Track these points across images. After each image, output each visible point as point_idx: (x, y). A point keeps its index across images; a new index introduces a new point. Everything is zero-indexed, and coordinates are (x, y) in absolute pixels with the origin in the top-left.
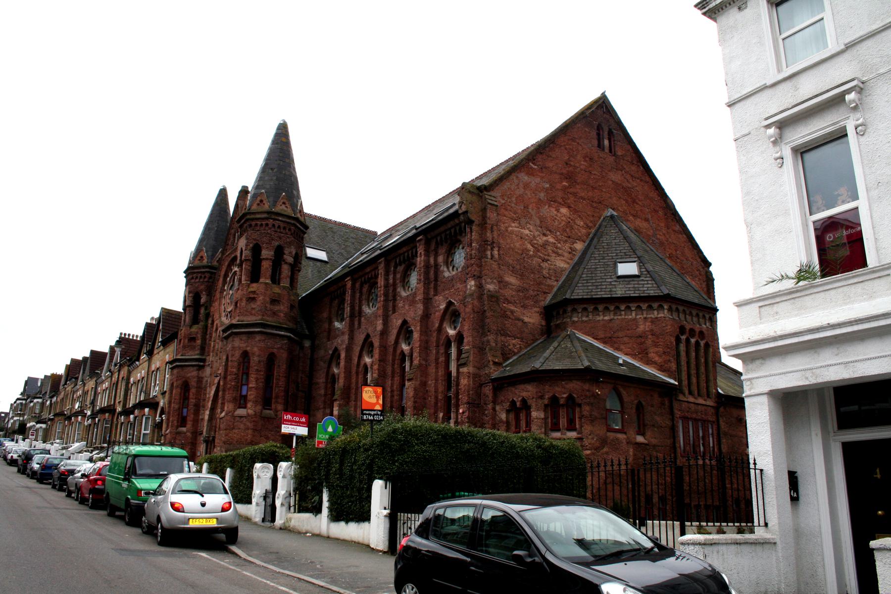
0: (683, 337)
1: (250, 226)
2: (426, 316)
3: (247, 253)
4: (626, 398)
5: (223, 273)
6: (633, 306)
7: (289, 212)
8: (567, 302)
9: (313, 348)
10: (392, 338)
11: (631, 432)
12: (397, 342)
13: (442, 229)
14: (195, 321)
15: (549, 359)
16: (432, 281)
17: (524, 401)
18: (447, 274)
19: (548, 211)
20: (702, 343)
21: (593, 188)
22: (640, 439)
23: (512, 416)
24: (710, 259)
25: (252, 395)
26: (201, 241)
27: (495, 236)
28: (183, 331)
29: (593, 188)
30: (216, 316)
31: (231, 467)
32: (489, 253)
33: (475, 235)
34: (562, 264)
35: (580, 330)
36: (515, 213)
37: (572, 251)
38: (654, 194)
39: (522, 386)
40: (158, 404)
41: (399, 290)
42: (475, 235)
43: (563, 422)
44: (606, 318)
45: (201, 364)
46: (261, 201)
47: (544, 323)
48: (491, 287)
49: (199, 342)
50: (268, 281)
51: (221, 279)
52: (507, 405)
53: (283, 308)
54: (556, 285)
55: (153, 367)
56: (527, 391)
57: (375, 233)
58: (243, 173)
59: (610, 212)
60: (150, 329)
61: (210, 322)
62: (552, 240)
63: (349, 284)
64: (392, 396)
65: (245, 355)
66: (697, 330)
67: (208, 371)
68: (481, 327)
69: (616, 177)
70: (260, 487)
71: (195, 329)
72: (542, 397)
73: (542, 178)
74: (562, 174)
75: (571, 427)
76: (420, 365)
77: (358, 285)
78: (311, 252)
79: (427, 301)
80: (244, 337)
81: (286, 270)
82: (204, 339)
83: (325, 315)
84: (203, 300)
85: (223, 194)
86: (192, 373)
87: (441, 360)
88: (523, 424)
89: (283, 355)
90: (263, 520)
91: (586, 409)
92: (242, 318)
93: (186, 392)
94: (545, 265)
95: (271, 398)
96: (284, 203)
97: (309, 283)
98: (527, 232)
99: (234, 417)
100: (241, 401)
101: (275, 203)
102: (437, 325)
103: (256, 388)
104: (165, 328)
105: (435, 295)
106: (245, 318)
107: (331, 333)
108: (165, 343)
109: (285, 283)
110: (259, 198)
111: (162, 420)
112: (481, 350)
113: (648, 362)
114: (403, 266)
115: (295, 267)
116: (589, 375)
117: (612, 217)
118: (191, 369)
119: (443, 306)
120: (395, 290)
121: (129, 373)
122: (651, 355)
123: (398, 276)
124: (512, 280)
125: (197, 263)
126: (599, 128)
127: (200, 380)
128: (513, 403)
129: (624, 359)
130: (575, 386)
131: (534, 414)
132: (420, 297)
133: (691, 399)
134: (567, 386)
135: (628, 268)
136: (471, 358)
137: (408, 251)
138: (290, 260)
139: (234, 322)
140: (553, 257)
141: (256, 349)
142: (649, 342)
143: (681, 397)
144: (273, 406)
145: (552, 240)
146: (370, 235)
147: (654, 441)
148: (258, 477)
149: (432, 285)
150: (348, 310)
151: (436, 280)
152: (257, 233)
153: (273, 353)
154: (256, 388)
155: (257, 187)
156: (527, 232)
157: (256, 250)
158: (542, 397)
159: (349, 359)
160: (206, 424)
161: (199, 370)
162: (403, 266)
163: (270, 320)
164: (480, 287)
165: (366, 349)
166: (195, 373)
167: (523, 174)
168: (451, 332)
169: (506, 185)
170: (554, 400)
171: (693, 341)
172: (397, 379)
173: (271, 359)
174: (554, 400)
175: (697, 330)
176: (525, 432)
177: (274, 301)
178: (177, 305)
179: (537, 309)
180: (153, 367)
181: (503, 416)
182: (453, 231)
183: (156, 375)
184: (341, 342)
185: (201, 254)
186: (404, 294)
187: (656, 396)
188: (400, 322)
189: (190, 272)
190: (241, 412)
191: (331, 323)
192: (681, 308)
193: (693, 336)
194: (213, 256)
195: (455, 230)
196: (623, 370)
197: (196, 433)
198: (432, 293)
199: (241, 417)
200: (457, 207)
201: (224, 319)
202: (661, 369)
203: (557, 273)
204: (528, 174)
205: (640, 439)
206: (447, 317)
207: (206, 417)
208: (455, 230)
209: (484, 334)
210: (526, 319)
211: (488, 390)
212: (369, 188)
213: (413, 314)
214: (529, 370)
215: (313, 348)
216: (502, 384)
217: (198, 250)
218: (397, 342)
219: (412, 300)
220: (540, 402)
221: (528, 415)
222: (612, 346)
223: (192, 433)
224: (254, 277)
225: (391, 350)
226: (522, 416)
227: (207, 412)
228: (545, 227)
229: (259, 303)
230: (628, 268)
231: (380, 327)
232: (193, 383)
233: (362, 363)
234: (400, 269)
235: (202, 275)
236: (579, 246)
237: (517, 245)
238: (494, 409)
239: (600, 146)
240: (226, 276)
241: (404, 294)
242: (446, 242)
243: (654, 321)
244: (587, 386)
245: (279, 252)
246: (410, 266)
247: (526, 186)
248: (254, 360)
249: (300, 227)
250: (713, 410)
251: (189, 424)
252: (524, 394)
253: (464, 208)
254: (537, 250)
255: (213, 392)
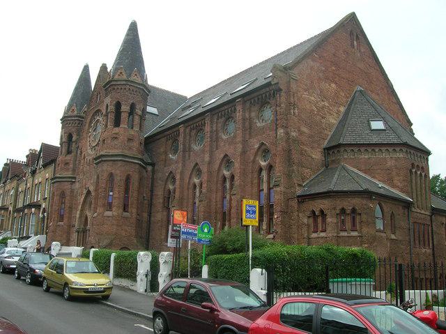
0: (414, 170)
1: (114, 89)
2: (244, 152)
3: (111, 108)
4: (385, 208)
5: (88, 121)
6: (384, 149)
7: (139, 81)
8: (339, 145)
9: (153, 172)
10: (216, 167)
11: (389, 232)
12: (219, 169)
13: (255, 94)
14: (69, 152)
15: (335, 183)
16: (249, 128)
17: (322, 212)
18: (258, 125)
19: (325, 85)
20: (423, 174)
21: (349, 72)
22: (393, 237)
23: (311, 220)
24: (412, 122)
25: (115, 202)
26: (72, 99)
27: (296, 100)
28: (60, 159)
29: (349, 72)
30: (84, 149)
31: (206, 263)
32: (292, 111)
33: (283, 99)
34: (333, 120)
35: (350, 164)
36: (306, 85)
37: (339, 111)
38: (381, 79)
39: (320, 201)
40: (40, 206)
41: (220, 134)
42: (283, 99)
43: (348, 225)
44: (366, 157)
45: (72, 180)
46: (121, 73)
47: (323, 159)
48: (294, 134)
49: (71, 166)
50: (126, 126)
51: (87, 125)
52: (308, 213)
53: (135, 144)
54: (330, 134)
55: (36, 181)
56: (319, 205)
57: (186, 97)
58: (105, 55)
59: (360, 88)
60: (33, 157)
61: (79, 152)
62: (327, 104)
63: (182, 130)
64: (216, 205)
65: (111, 175)
66: (421, 167)
67: (77, 185)
68: (289, 160)
69: (361, 65)
70: (143, 267)
71: (69, 157)
72: (335, 209)
73: (321, 63)
74: (332, 62)
75: (354, 229)
76: (240, 185)
77: (188, 130)
78: (149, 109)
79: (245, 142)
80: (110, 163)
81: (137, 119)
82: (75, 164)
83: (162, 150)
84: (74, 139)
85: (86, 69)
86: (67, 186)
87: (254, 182)
88: (320, 226)
89: (135, 178)
90: (146, 291)
91: (364, 217)
92: (108, 151)
93: (62, 198)
94: (323, 121)
95: (128, 205)
96: (136, 75)
97: (151, 130)
98: (313, 98)
99: (103, 216)
100: (109, 206)
101: (130, 75)
102: (252, 159)
103: (119, 198)
104: (44, 157)
105: (250, 138)
106: (110, 151)
107: (166, 162)
108: (45, 166)
109: (136, 128)
110: (119, 71)
111: (44, 216)
112: (289, 176)
113: (394, 186)
114: (223, 119)
115: (142, 118)
116: (367, 194)
117: (361, 91)
118: (66, 183)
119: (257, 146)
120: (217, 134)
121: (18, 185)
122: (395, 182)
123: (220, 125)
124: (305, 129)
125: (70, 113)
126: (351, 34)
127: (72, 191)
128: (313, 212)
129: (381, 186)
130: (356, 202)
131: (329, 220)
132: (239, 139)
133: (419, 211)
134: (352, 202)
135: (377, 125)
136: (282, 181)
137: (228, 109)
138: (140, 113)
139: (102, 153)
140: (328, 116)
141: (118, 172)
142: (394, 173)
143: (413, 209)
144: (130, 210)
145: (327, 104)
146: (183, 99)
147: (400, 238)
148: (142, 261)
149: (248, 132)
150: (181, 147)
151: (250, 128)
152: (113, 98)
153: (129, 175)
154: (119, 198)
155: (116, 69)
156: (313, 98)
157: (118, 105)
158: (335, 209)
159: (182, 179)
160: (77, 220)
161: (71, 184)
162: (223, 119)
163: (127, 153)
164: (287, 133)
165: (194, 173)
166: (69, 186)
167: (310, 60)
168: (263, 164)
169: (301, 66)
170: (343, 211)
171: (419, 173)
172: (220, 194)
173: (128, 178)
174: (343, 211)
175: (421, 167)
176: (322, 231)
177: (129, 140)
178: (55, 140)
179: (320, 150)
180: (36, 181)
181: (305, 221)
182: (264, 95)
183: (41, 187)
184: (177, 168)
185: (73, 108)
186: (224, 137)
187: (401, 208)
188: (222, 156)
189: (65, 120)
190: (108, 213)
191: (166, 153)
192: (412, 152)
193: (418, 170)
194: (81, 110)
195: (266, 96)
196: (382, 191)
197: (71, 226)
198: (248, 136)
199: (109, 217)
200: (270, 79)
201: (90, 151)
202: (402, 191)
203: (330, 125)
204: (313, 60)
205: (393, 237)
206: (260, 153)
207: (78, 216)
208: (266, 96)
209: (290, 165)
210: (314, 156)
211: (294, 203)
212: (186, 69)
213: (234, 151)
214: (325, 190)
215: (153, 172)
216: (303, 199)
217: (70, 105)
218: (219, 169)
219: (232, 142)
220: (333, 212)
221: (324, 221)
222: (370, 175)
223: (68, 226)
224: (117, 123)
225: (215, 174)
226: (320, 220)
227: (78, 212)
228: (324, 97)
229: (120, 141)
230: (377, 125)
231: (207, 158)
232: (68, 193)
233: (192, 182)
234: (222, 120)
235: (74, 123)
236: (342, 109)
237: (308, 107)
238: (298, 216)
239: (353, 46)
240: (91, 122)
241: (224, 137)
242: (258, 103)
243: (397, 159)
244: (365, 202)
245: (133, 107)
246: (229, 118)
247: (312, 68)
248: (117, 179)
249: (146, 92)
250: (429, 217)
251: (66, 220)
252: (322, 206)
253: (275, 81)
254: (319, 111)
255: (82, 199)
